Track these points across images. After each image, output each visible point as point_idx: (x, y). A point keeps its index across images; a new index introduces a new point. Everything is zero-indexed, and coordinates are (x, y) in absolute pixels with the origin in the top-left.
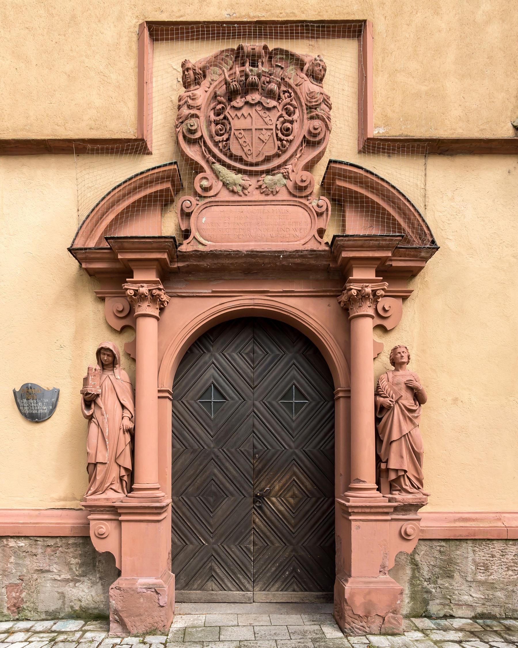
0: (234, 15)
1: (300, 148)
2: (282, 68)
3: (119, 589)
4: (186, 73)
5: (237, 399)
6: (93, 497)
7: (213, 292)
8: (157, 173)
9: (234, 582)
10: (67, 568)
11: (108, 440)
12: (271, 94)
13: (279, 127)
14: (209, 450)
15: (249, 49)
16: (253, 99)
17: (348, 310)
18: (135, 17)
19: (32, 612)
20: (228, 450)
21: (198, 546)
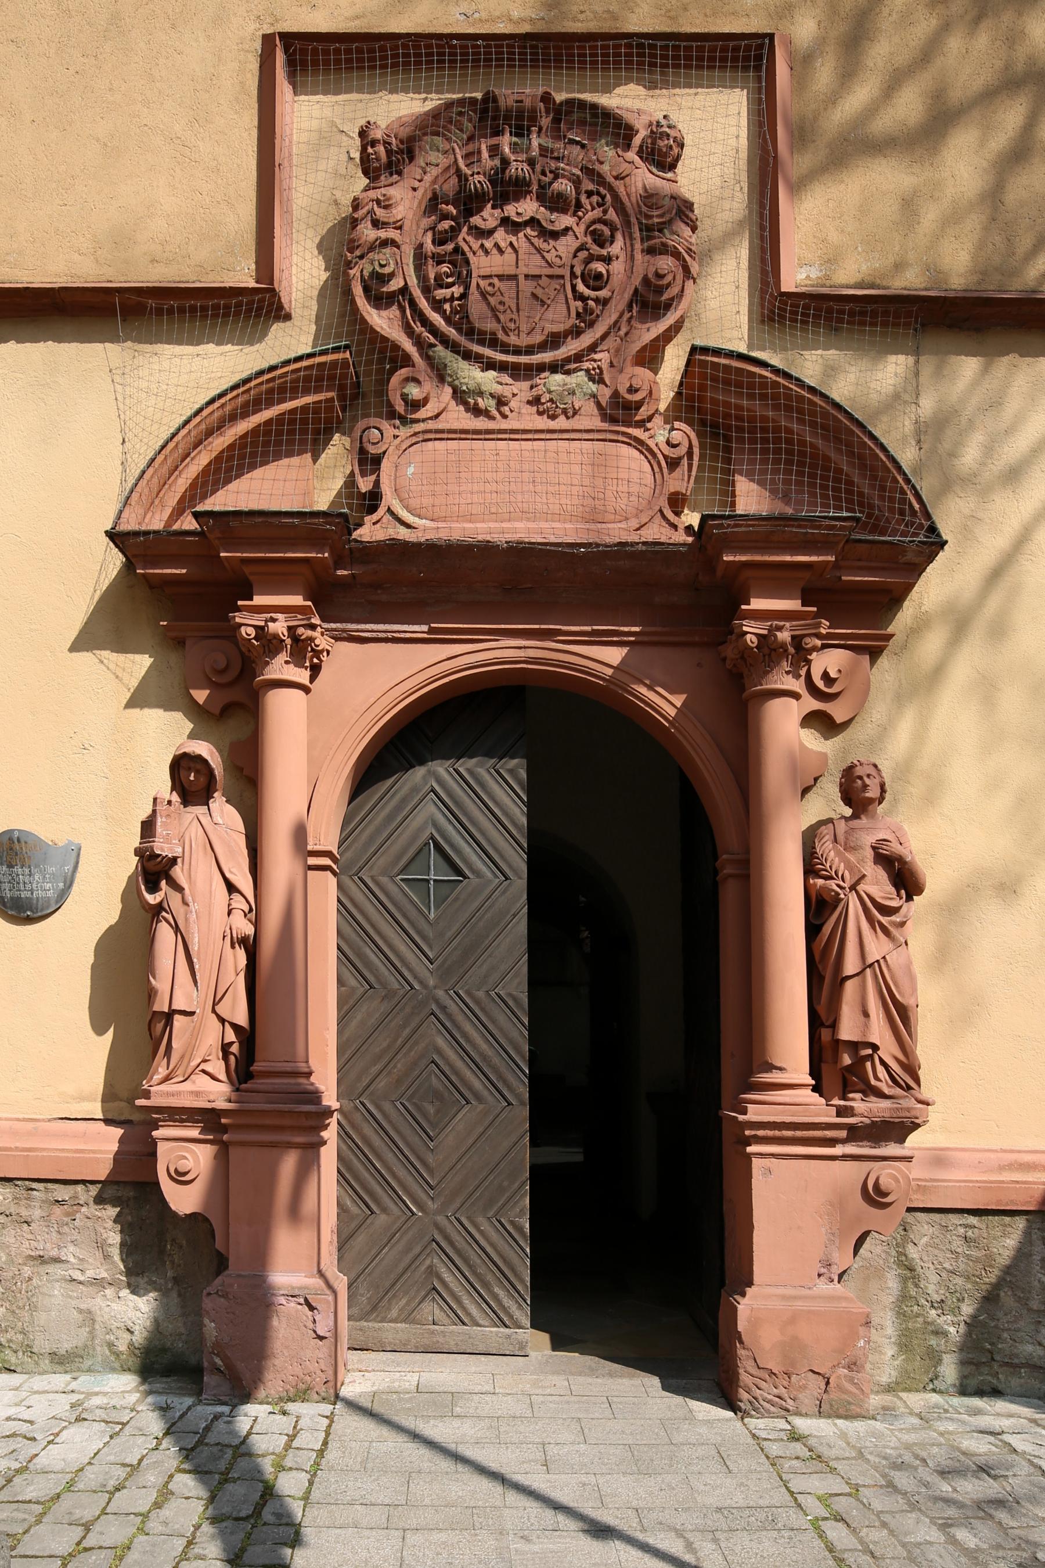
0: (477, 15)
1: (627, 315)
2: (583, 146)
3: (225, 1296)
4: (370, 150)
5: (489, 874)
6: (163, 1087)
7: (431, 631)
8: (306, 368)
9: (484, 1306)
10: (99, 1255)
11: (198, 959)
12: (557, 203)
13: (578, 271)
14: (424, 992)
15: (510, 102)
16: (518, 214)
17: (741, 676)
18: (252, 18)
19: (20, 1354)
20: (468, 993)
21: (399, 1218)
